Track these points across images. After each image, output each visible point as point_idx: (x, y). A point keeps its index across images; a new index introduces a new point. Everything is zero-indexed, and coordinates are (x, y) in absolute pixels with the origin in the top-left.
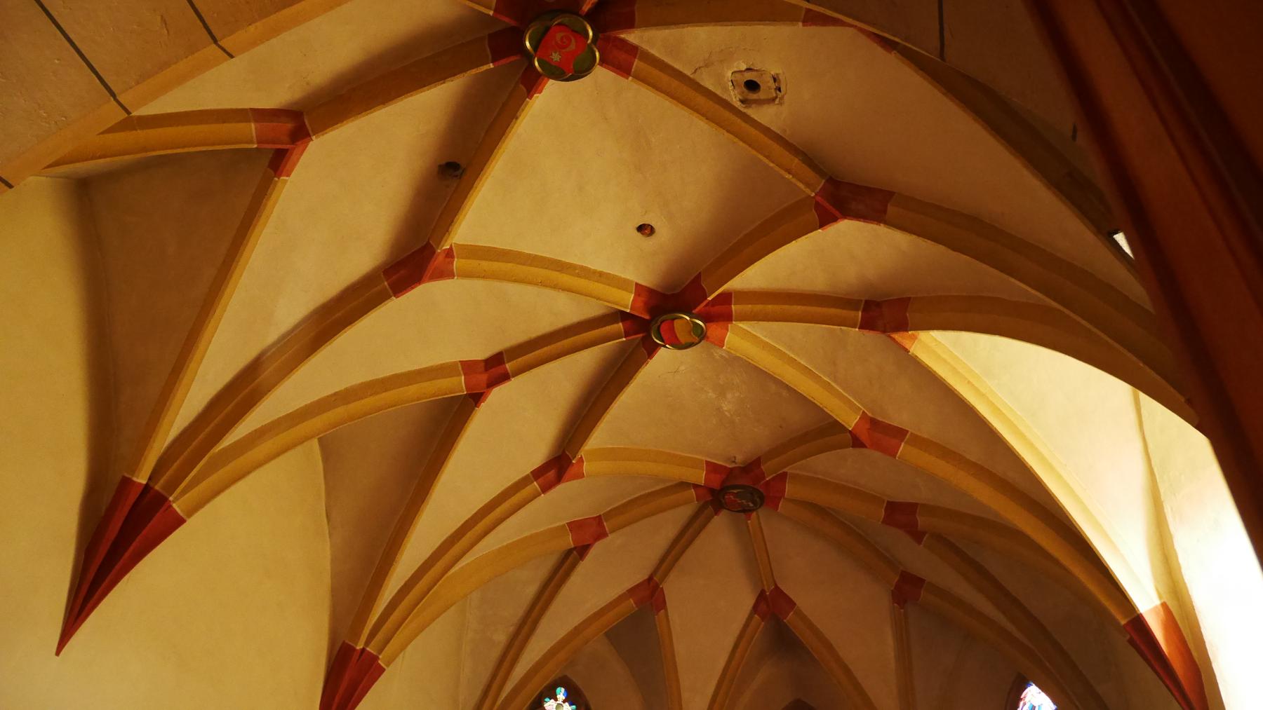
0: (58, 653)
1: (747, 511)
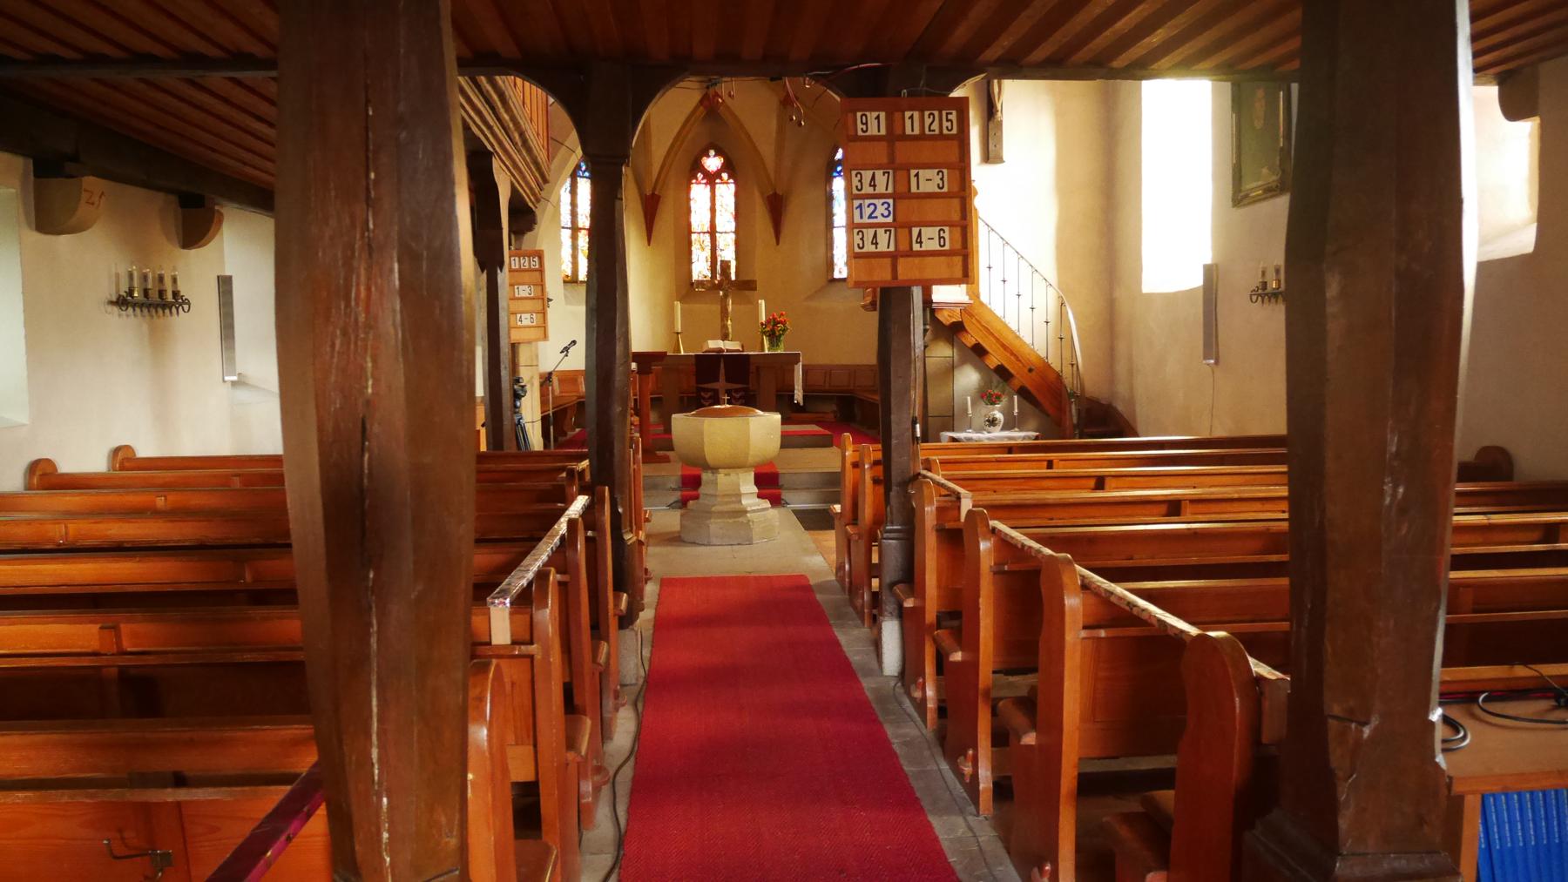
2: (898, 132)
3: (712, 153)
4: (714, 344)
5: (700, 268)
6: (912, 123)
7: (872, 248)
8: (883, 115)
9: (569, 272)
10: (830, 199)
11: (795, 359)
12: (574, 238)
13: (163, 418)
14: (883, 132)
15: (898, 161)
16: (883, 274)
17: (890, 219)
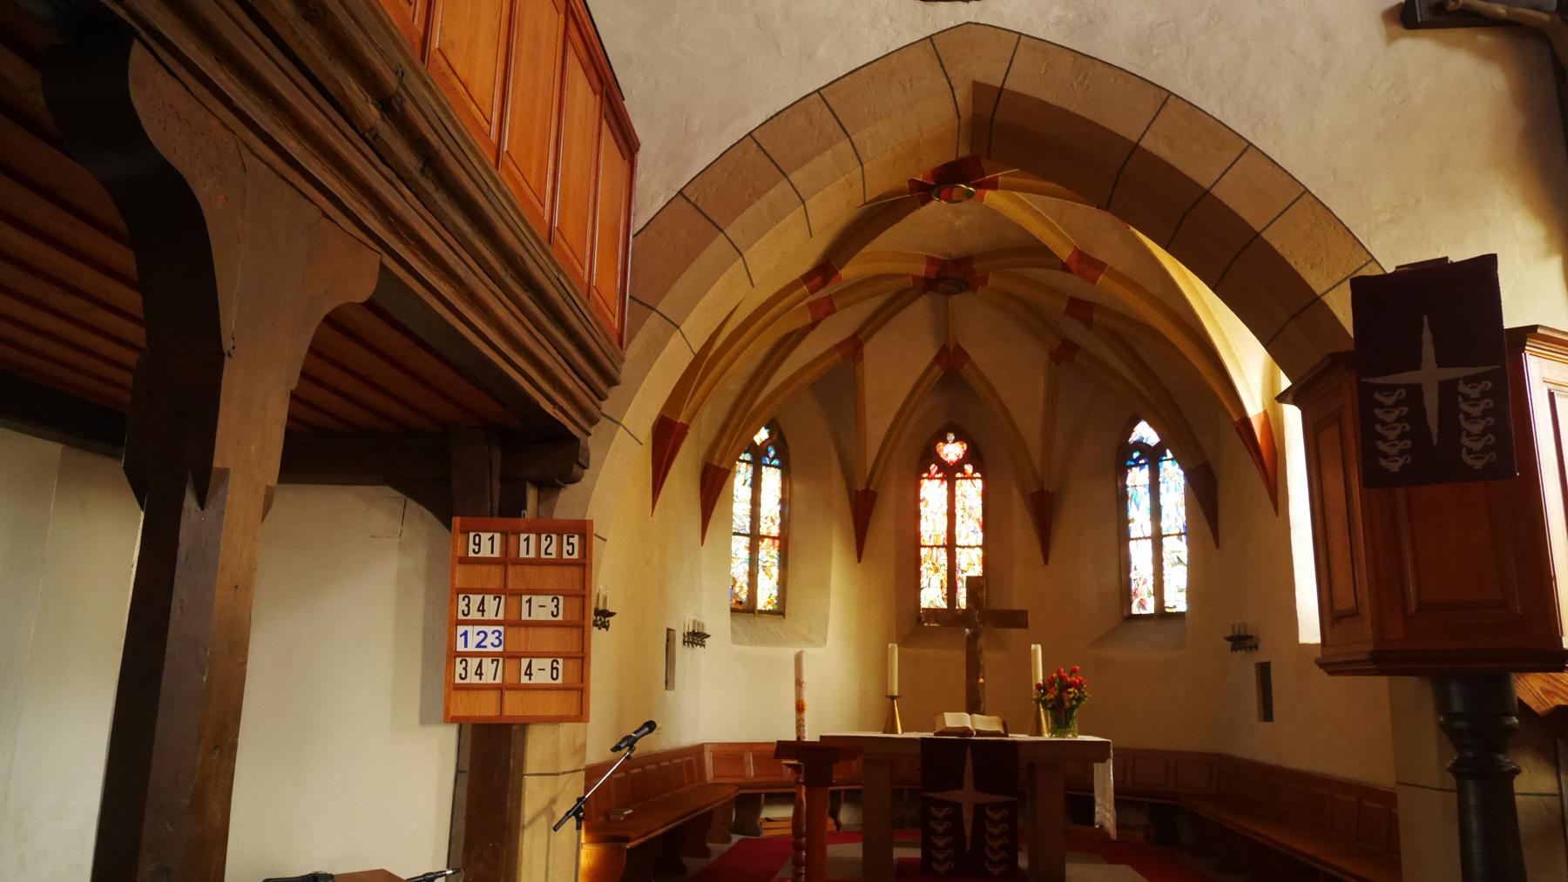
0: (1046, 562)
1: (950, 293)
2: (512, 554)
3: (951, 437)
4: (955, 720)
5: (932, 595)
6: (527, 547)
7: (475, 680)
8: (497, 536)
9: (744, 597)
10: (1122, 498)
11: (1097, 752)
12: (753, 549)
13: (583, 759)
14: (497, 554)
15: (510, 586)
16: (485, 708)
17: (500, 649)
